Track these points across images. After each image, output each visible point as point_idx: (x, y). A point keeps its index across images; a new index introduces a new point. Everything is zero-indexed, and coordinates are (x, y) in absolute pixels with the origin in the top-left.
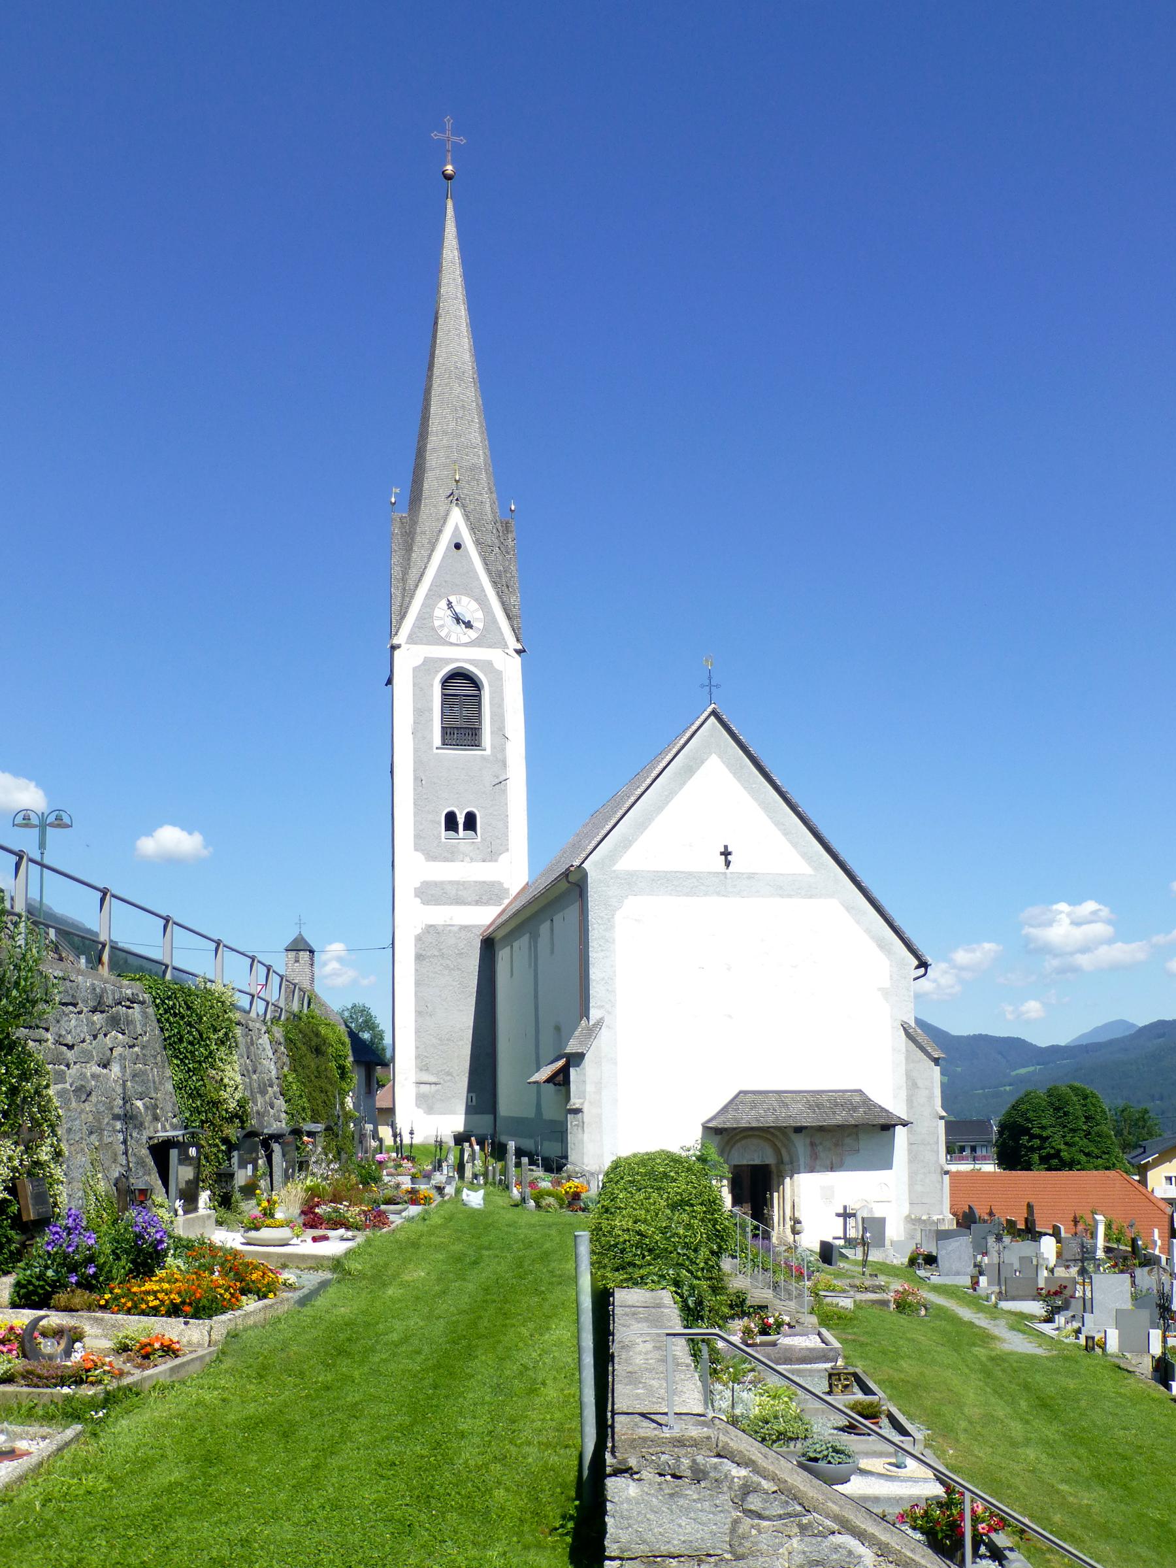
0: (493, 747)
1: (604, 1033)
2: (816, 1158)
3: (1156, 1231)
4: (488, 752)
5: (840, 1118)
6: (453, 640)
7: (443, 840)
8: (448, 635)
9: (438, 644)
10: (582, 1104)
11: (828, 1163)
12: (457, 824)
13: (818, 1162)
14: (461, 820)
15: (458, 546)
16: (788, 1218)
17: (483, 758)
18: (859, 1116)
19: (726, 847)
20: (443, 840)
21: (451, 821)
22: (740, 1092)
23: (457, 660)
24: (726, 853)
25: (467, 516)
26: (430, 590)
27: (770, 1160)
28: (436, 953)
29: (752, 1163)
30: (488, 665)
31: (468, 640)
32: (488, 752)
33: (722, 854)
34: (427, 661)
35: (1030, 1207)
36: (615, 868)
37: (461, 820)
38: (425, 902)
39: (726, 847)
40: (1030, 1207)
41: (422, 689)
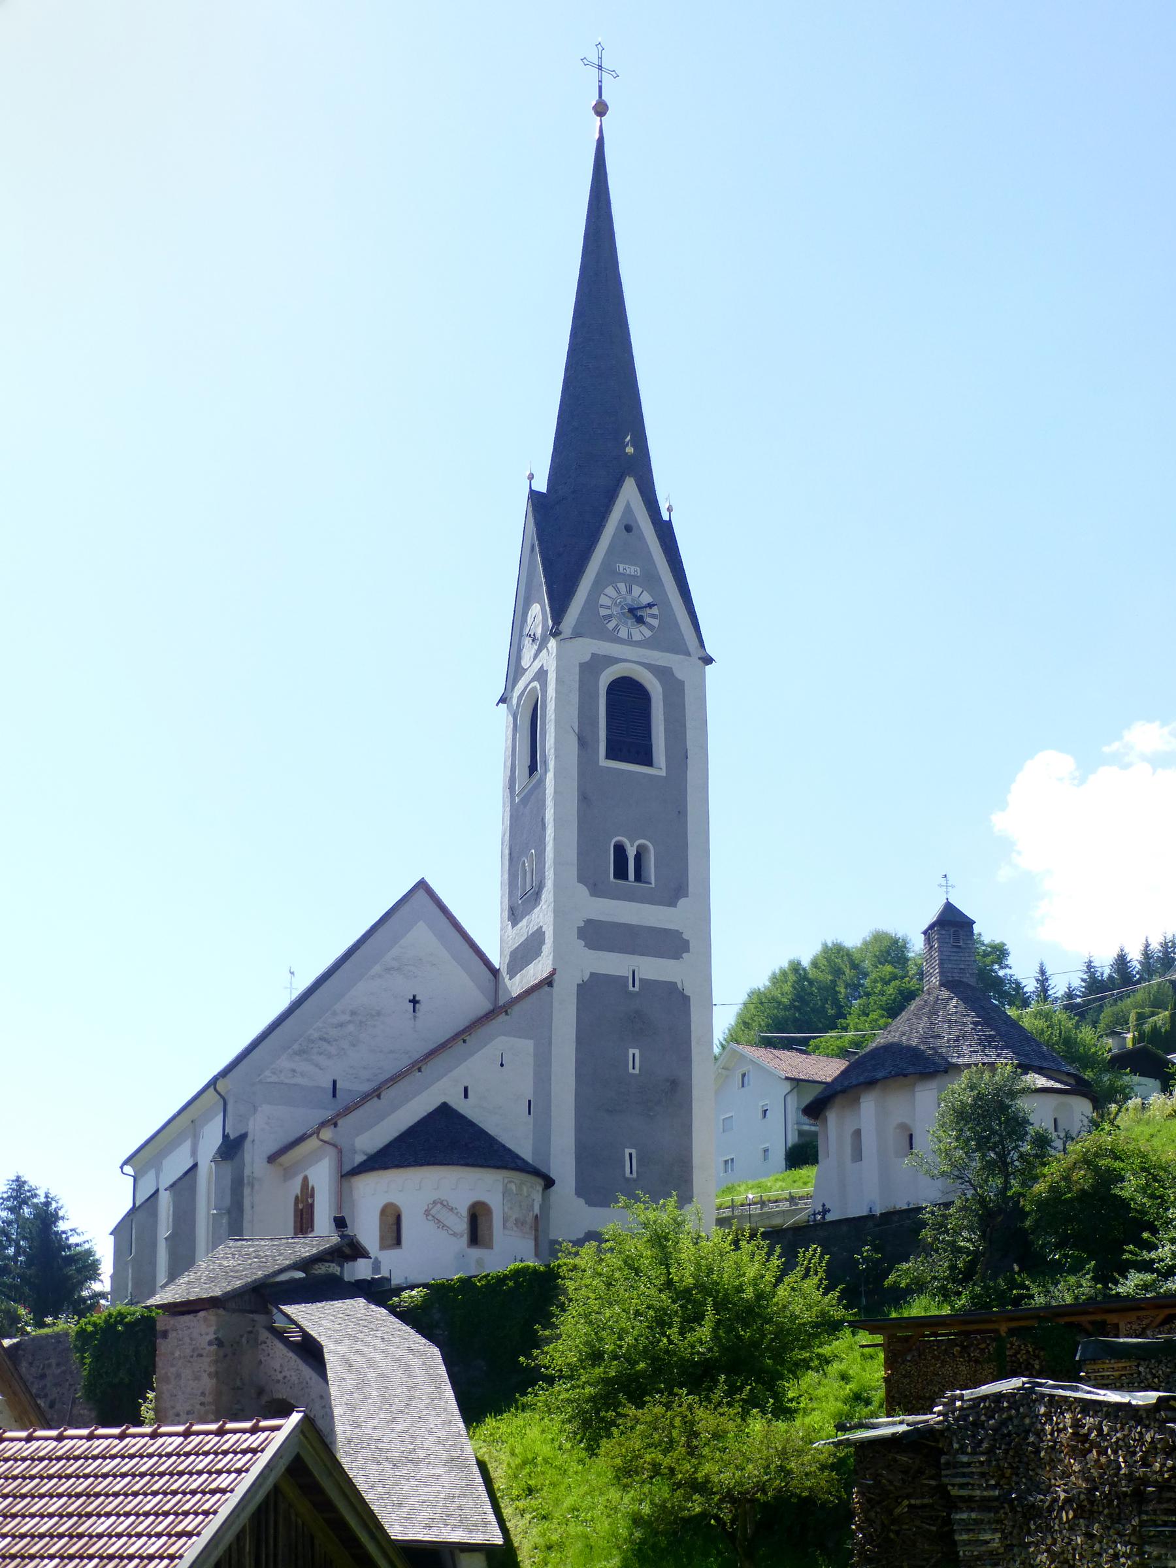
14: (631, 853)
15: (628, 529)
19: (414, 997)
39: (414, 997)
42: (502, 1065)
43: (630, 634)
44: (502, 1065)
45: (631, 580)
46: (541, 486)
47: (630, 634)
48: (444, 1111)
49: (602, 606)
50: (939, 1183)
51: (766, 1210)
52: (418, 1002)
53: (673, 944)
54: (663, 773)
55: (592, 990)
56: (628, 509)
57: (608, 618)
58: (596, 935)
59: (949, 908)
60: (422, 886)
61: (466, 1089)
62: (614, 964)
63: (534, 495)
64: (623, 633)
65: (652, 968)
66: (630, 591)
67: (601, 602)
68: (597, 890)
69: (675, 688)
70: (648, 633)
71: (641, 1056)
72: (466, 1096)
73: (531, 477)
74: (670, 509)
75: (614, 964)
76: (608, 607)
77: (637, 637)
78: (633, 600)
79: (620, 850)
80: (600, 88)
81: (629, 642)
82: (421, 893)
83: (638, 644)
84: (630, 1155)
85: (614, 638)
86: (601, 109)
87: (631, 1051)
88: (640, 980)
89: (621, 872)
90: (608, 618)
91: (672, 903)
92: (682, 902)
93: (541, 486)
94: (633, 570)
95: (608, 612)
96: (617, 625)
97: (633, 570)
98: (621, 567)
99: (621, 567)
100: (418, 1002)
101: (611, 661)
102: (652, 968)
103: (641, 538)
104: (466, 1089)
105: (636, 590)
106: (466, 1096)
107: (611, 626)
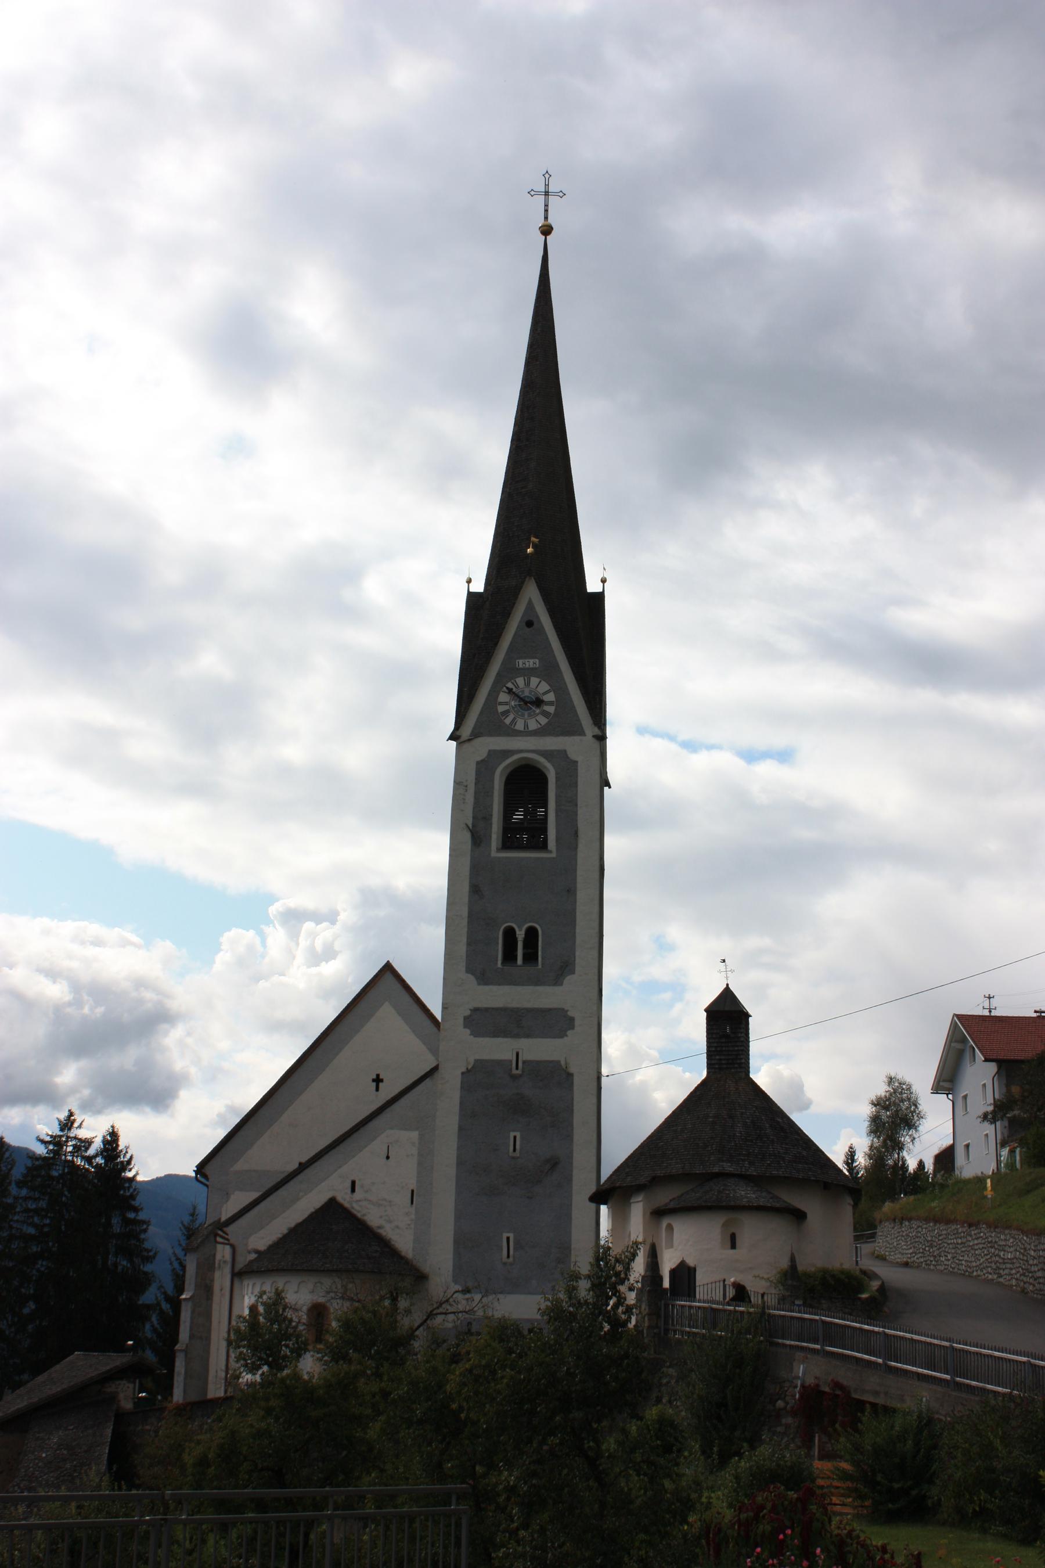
8: (513, 721)
14: (520, 934)
15: (529, 624)
19: (378, 1075)
23: (521, 751)
30: (559, 757)
33: (374, 1080)
37: (520, 934)
38: (475, 1034)
39: (378, 1075)
42: (388, 1158)
43: (526, 725)
44: (388, 1158)
45: (528, 673)
46: (478, 586)
47: (526, 725)
48: (332, 1204)
49: (501, 704)
50: (763, 1283)
51: (1001, 1280)
52: (382, 1081)
53: (555, 1022)
54: (554, 855)
55: (479, 1077)
56: (530, 605)
57: (506, 713)
58: (483, 1022)
59: (727, 995)
60: (388, 969)
61: (353, 1183)
62: (500, 1049)
63: (472, 597)
64: (520, 726)
65: (538, 1049)
66: (528, 684)
67: (532, 679)
68: (484, 978)
69: (569, 768)
70: (543, 721)
71: (522, 1138)
72: (353, 1190)
73: (469, 581)
74: (52, 974)
75: (500, 1049)
76: (506, 703)
77: (533, 725)
78: (530, 692)
79: (510, 935)
80: (546, 211)
81: (527, 733)
82: (389, 976)
83: (536, 733)
84: (508, 1239)
85: (511, 732)
86: (546, 230)
87: (512, 1134)
88: (524, 1062)
89: (509, 955)
90: (506, 713)
91: (557, 981)
92: (568, 980)
93: (478, 586)
94: (531, 663)
95: (506, 708)
96: (514, 719)
97: (531, 663)
98: (521, 663)
99: (521, 663)
100: (382, 1081)
101: (506, 753)
102: (538, 1049)
103: (541, 631)
104: (353, 1183)
105: (534, 681)
106: (353, 1190)
107: (508, 721)
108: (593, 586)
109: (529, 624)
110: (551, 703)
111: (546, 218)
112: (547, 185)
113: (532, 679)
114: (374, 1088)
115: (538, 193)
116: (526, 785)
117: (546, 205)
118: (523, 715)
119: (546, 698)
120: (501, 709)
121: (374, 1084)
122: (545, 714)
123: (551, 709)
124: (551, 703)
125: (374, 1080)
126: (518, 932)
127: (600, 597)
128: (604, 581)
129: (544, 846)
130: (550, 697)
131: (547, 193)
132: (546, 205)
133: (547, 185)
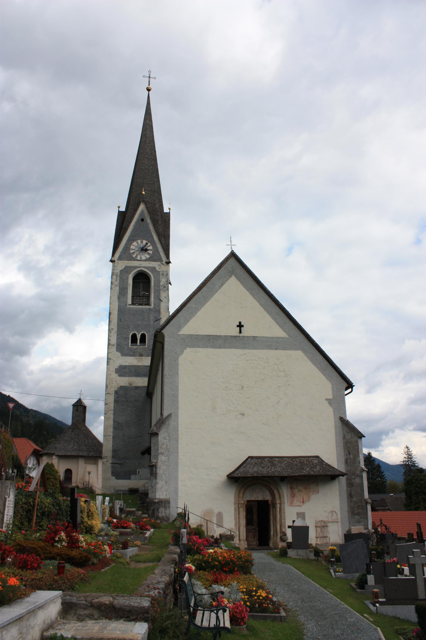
0: (154, 304)
1: (171, 422)
2: (293, 497)
3: (378, 590)
4: (152, 306)
5: (306, 471)
6: (139, 258)
7: (130, 346)
8: (136, 256)
9: (131, 260)
10: (157, 462)
11: (301, 499)
12: (136, 339)
13: (295, 499)
14: (139, 337)
15: (142, 220)
16: (279, 532)
17: (150, 309)
18: (317, 470)
19: (240, 323)
20: (130, 346)
21: (134, 338)
22: (249, 457)
23: (140, 267)
24: (240, 326)
25: (147, 208)
26: (129, 238)
27: (268, 498)
28: (124, 400)
29: (257, 499)
30: (153, 269)
31: (145, 258)
32: (152, 306)
33: (238, 326)
34: (126, 267)
35: (419, 526)
36: (180, 333)
37: (139, 337)
38: (120, 375)
39: (240, 323)
40: (419, 526)
41: (123, 279)
47: (141, 258)
52: (243, 326)
63: (120, 212)
70: (148, 256)
73: (119, 207)
76: (134, 249)
77: (144, 258)
83: (146, 260)
85: (135, 259)
93: (123, 209)
95: (134, 251)
100: (243, 326)
101: (136, 267)
108: (166, 210)
109: (142, 220)
110: (151, 250)
111: (149, 85)
112: (150, 75)
113: (144, 241)
114: (239, 331)
115: (146, 77)
116: (142, 280)
117: (149, 81)
118: (140, 254)
119: (149, 248)
120: (132, 251)
121: (238, 328)
122: (149, 254)
123: (151, 252)
124: (151, 250)
125: (238, 326)
126: (137, 335)
127: (168, 214)
128: (169, 209)
129: (148, 304)
130: (151, 248)
131: (149, 77)
132: (149, 81)
133: (150, 75)
